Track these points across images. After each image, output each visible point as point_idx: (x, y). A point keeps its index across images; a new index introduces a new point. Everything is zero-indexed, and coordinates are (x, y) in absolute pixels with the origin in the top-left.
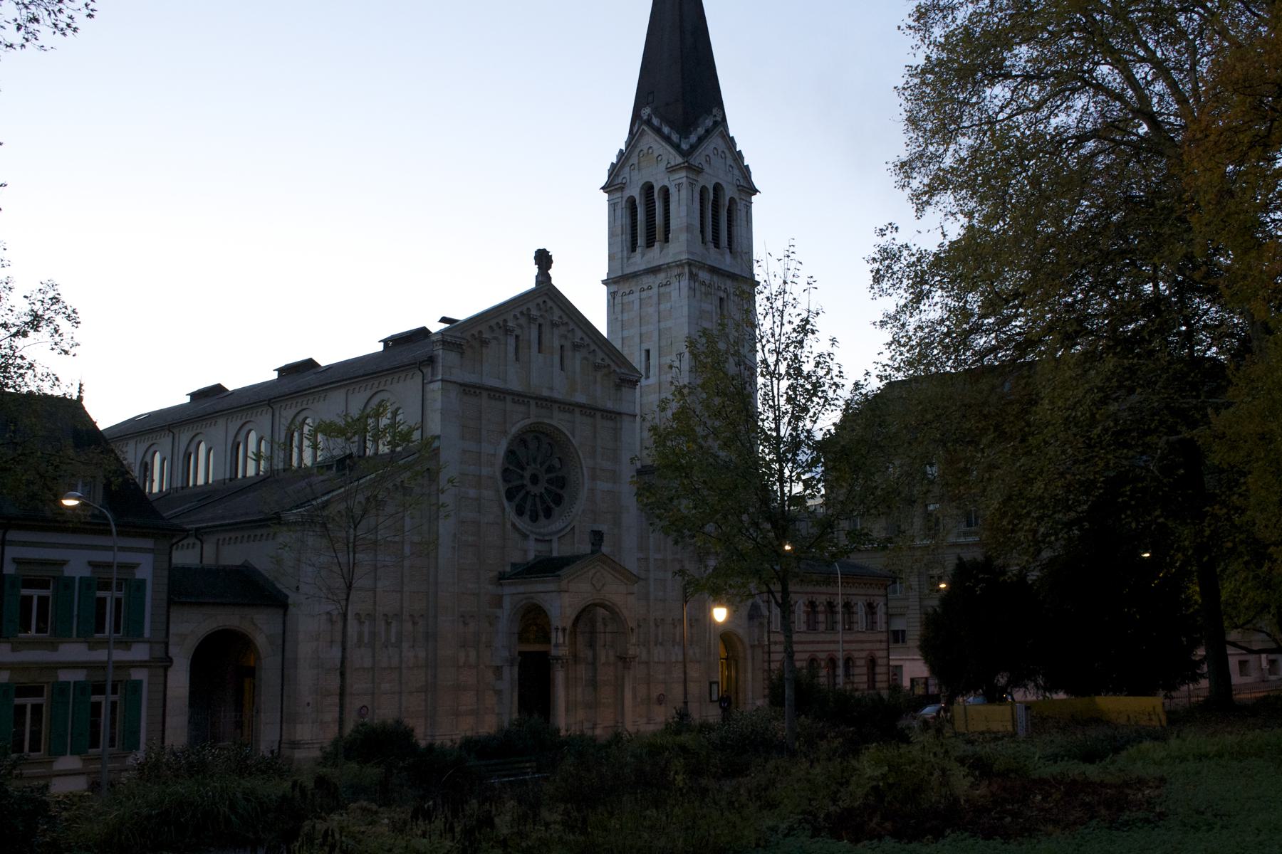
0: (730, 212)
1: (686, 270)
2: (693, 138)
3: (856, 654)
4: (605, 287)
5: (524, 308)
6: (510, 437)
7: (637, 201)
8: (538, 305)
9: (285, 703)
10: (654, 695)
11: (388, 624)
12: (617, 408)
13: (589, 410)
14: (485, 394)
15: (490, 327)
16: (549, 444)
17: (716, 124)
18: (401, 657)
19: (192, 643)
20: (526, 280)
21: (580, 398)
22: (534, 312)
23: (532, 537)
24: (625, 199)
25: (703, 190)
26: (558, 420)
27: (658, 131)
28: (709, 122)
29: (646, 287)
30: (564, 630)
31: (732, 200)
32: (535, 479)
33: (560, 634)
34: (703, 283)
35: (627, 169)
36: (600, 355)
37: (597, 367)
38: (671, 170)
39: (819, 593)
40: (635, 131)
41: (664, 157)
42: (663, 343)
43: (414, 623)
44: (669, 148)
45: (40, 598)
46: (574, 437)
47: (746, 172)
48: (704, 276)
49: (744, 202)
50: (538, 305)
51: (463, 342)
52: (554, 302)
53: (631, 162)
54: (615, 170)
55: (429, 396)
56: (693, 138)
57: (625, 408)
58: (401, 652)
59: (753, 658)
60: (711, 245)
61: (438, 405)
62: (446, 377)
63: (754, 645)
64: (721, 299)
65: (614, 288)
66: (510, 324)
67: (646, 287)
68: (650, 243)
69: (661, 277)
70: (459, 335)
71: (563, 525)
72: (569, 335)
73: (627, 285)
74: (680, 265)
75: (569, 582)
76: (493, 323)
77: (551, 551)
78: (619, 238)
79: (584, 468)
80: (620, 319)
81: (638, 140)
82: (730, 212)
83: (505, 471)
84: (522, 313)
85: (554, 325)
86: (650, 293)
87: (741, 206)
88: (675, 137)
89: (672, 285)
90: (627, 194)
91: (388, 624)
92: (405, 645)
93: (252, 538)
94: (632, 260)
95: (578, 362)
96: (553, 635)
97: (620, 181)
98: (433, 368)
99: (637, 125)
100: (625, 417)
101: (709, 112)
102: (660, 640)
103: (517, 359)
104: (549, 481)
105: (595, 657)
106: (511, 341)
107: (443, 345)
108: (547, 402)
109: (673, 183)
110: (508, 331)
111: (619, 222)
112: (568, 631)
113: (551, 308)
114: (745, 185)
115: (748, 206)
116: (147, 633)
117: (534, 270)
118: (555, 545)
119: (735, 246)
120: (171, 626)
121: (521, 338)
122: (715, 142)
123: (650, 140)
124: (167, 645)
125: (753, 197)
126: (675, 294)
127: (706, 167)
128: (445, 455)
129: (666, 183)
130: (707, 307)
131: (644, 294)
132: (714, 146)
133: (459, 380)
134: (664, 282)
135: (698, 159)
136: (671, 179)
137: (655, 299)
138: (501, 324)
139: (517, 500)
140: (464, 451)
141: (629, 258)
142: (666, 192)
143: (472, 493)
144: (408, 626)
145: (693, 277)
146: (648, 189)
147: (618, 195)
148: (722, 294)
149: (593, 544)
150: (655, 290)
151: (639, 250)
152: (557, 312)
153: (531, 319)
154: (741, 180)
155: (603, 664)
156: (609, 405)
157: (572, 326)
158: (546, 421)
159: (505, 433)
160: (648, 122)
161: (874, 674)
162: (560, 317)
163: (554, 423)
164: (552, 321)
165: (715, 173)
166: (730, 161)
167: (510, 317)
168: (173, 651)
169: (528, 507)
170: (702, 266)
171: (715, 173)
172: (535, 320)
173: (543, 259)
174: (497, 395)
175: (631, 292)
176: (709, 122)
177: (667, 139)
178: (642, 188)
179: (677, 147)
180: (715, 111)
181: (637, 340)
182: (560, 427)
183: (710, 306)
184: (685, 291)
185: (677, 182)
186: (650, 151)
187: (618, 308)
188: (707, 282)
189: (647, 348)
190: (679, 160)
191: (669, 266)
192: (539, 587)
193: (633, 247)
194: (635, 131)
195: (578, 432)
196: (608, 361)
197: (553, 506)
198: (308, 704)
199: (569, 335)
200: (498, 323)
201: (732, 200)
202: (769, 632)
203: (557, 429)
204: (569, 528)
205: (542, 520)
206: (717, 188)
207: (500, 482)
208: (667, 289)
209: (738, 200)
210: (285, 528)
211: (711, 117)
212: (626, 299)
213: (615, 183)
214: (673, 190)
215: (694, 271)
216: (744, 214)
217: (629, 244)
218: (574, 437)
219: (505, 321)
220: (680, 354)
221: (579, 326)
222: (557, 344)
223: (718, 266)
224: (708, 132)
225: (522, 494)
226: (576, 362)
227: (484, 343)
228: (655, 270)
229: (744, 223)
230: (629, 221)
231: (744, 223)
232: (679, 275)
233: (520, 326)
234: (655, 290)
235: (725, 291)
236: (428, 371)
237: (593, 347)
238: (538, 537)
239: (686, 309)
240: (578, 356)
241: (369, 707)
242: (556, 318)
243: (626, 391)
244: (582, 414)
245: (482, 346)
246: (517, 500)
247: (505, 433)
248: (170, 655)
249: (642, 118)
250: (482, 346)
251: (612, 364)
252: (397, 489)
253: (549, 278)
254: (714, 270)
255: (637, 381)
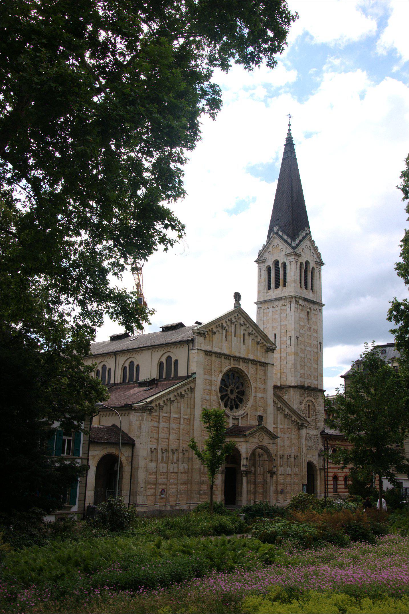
0: (312, 273)
1: (294, 299)
2: (297, 241)
3: (339, 474)
4: (256, 305)
5: (229, 318)
6: (223, 373)
7: (271, 268)
8: (235, 316)
9: (132, 486)
10: (279, 489)
11: (173, 453)
12: (266, 361)
13: (254, 362)
14: (223, 357)
15: (216, 326)
16: (238, 376)
17: (307, 234)
18: (178, 468)
19: (97, 459)
20: (229, 306)
21: (251, 357)
22: (233, 320)
23: (231, 417)
24: (265, 266)
25: (301, 264)
26: (242, 366)
27: (281, 237)
28: (304, 234)
29: (275, 306)
30: (247, 459)
31: (313, 268)
32: (232, 392)
33: (245, 460)
34: (301, 305)
35: (266, 254)
36: (259, 338)
37: (258, 343)
38: (288, 255)
39: (349, 446)
40: (271, 237)
41: (284, 250)
42: (282, 331)
43: (184, 454)
44: (287, 245)
45: (68, 440)
46: (248, 373)
47: (319, 256)
48: (301, 302)
49: (318, 269)
50: (235, 316)
51: (206, 333)
52: (242, 315)
53: (269, 250)
54: (261, 254)
55: (191, 355)
56: (297, 241)
57: (269, 361)
58: (178, 466)
59: (320, 475)
60: (304, 288)
61: (195, 359)
62: (199, 348)
63: (321, 468)
64: (308, 312)
65: (260, 306)
66: (224, 325)
67: (275, 306)
68: (277, 286)
69: (282, 302)
70: (204, 330)
71: (243, 412)
72: (247, 329)
73: (266, 305)
74: (291, 297)
75: (249, 438)
76: (217, 324)
77: (238, 423)
78: (263, 284)
79: (252, 387)
80: (262, 319)
81: (272, 242)
82: (312, 273)
83: (221, 387)
84: (229, 320)
85: (241, 325)
86: (277, 309)
87: (317, 270)
88: (289, 241)
89: (287, 306)
90: (266, 265)
91: (173, 453)
92: (180, 463)
93: (111, 415)
94: (269, 294)
95: (250, 341)
96: (242, 460)
97: (263, 259)
98: (193, 343)
99: (272, 235)
100: (269, 365)
101: (304, 230)
102: (282, 465)
103: (226, 340)
104: (238, 393)
105: (255, 470)
106: (224, 332)
107: (198, 334)
108: (238, 359)
109: (288, 261)
110: (223, 328)
111: (262, 277)
112: (248, 460)
113: (240, 318)
114: (319, 261)
115: (320, 271)
116: (81, 455)
117: (233, 301)
118: (240, 421)
119: (314, 288)
120: (90, 452)
121: (228, 331)
122: (306, 242)
123: (277, 241)
124: (88, 460)
125: (322, 267)
126: (288, 310)
127: (302, 254)
128: (198, 381)
129: (285, 261)
130: (302, 316)
131: (274, 309)
132: (306, 244)
133: (204, 349)
134: (283, 304)
135: (299, 250)
136: (287, 259)
137: (279, 312)
138: (221, 325)
139: (225, 400)
140: (205, 379)
141: (267, 293)
142: (285, 265)
143: (208, 397)
144: (181, 455)
145: (296, 302)
146: (277, 263)
147: (262, 265)
148: (309, 310)
149: (259, 421)
150: (279, 308)
151: (272, 289)
152: (243, 320)
153: (232, 323)
154: (317, 259)
155: (259, 474)
156: (263, 360)
157: (248, 325)
158: (237, 366)
159: (221, 372)
160: (277, 233)
161: (337, 484)
162: (244, 322)
163: (241, 367)
164: (240, 323)
165: (307, 256)
166: (312, 251)
167: (224, 322)
168: (90, 463)
169: (229, 403)
170: (300, 298)
171: (307, 256)
172: (234, 323)
173: (237, 297)
174: (209, 353)
175: (268, 308)
176: (304, 234)
177: (286, 241)
178: (273, 262)
179: (290, 245)
180: (306, 229)
181: (270, 329)
182: (243, 369)
183: (304, 315)
184: (293, 309)
185: (290, 260)
186: (278, 246)
187: (262, 315)
188: (302, 305)
189: (275, 333)
190: (291, 251)
191: (286, 298)
192: (236, 440)
193: (269, 288)
194: (271, 237)
195: (250, 371)
196: (262, 341)
197: (239, 404)
198: (142, 487)
199: (247, 329)
200: (219, 325)
201: (313, 268)
202: (327, 463)
203: (241, 370)
204: (245, 414)
205: (235, 410)
206: (307, 263)
207: (219, 393)
208: (285, 308)
209: (315, 268)
210: (134, 412)
211: (304, 231)
212: (265, 311)
213: (262, 259)
214: (288, 264)
215: (297, 300)
216: (318, 276)
217: (267, 286)
218: (248, 373)
219: (222, 323)
220: (291, 337)
221: (251, 326)
222: (242, 334)
223: (307, 298)
224: (304, 238)
225: (227, 398)
226: (249, 341)
227: (213, 333)
228: (279, 299)
229: (318, 278)
230: (267, 277)
231: (318, 278)
232: (290, 302)
233: (228, 326)
234: (279, 308)
235: (310, 309)
236: (191, 345)
237: (256, 334)
238: (234, 417)
239: (293, 317)
240: (251, 338)
241: (165, 489)
242: (242, 322)
243: (270, 353)
244: (243, 362)
245: (213, 334)
246: (225, 400)
247: (221, 372)
248: (89, 464)
249: (274, 231)
250: (213, 334)
251: (264, 342)
252: (178, 396)
253: (240, 305)
254: (305, 300)
255: (274, 349)
